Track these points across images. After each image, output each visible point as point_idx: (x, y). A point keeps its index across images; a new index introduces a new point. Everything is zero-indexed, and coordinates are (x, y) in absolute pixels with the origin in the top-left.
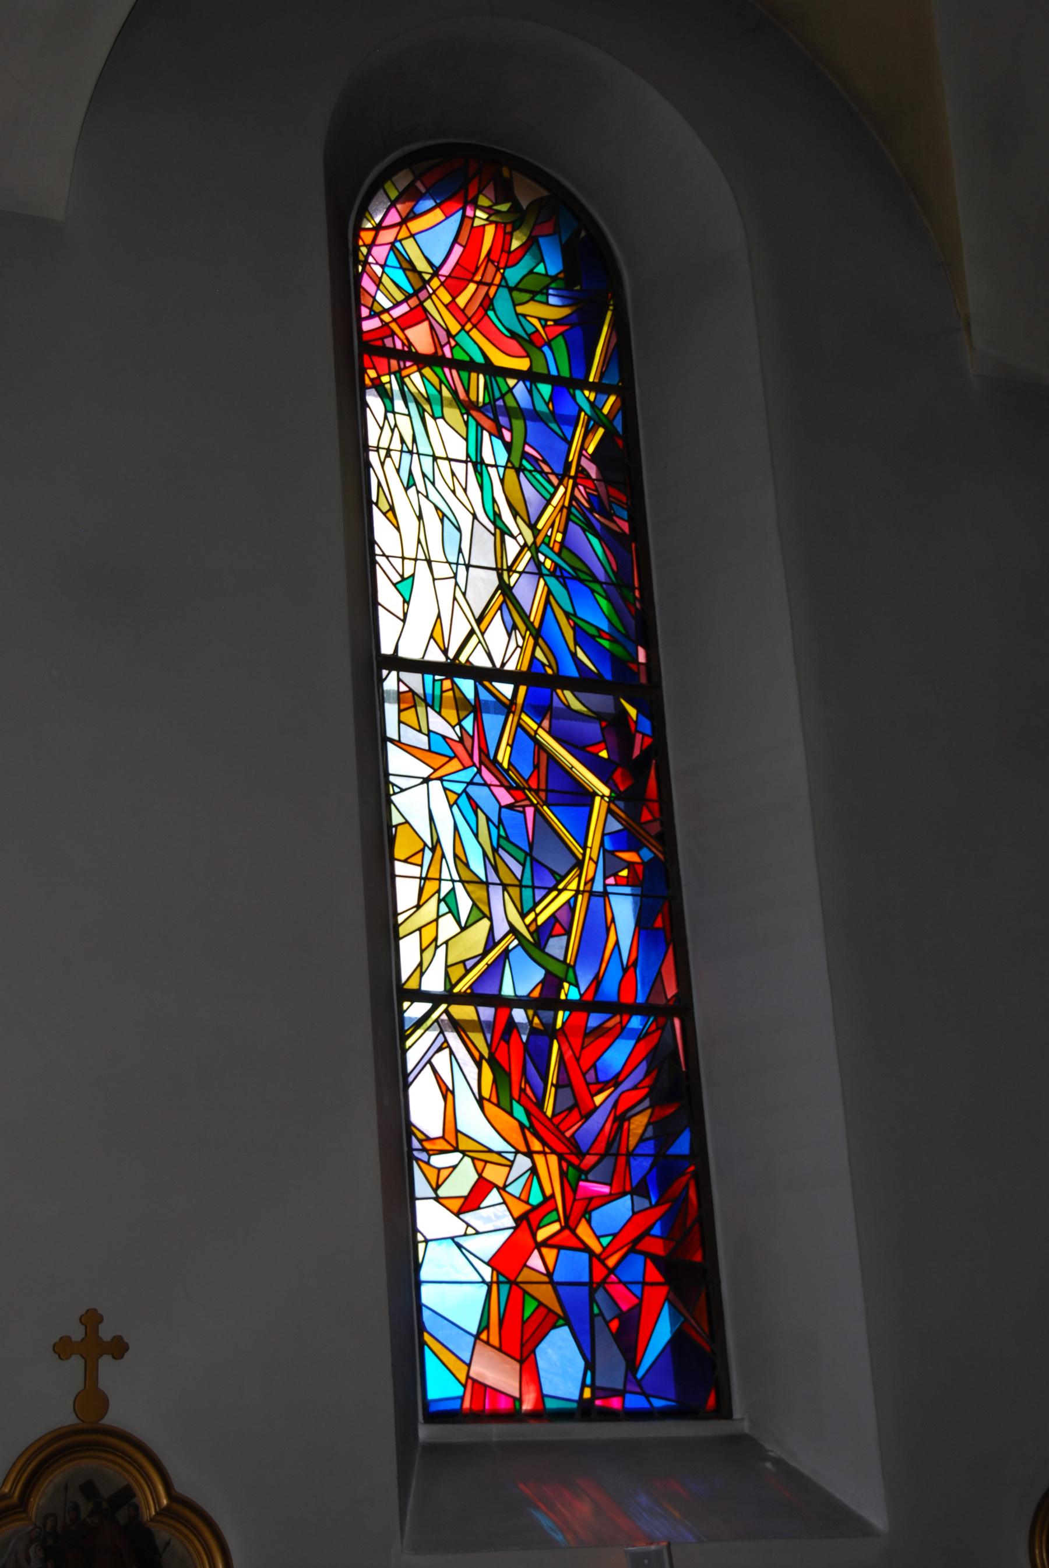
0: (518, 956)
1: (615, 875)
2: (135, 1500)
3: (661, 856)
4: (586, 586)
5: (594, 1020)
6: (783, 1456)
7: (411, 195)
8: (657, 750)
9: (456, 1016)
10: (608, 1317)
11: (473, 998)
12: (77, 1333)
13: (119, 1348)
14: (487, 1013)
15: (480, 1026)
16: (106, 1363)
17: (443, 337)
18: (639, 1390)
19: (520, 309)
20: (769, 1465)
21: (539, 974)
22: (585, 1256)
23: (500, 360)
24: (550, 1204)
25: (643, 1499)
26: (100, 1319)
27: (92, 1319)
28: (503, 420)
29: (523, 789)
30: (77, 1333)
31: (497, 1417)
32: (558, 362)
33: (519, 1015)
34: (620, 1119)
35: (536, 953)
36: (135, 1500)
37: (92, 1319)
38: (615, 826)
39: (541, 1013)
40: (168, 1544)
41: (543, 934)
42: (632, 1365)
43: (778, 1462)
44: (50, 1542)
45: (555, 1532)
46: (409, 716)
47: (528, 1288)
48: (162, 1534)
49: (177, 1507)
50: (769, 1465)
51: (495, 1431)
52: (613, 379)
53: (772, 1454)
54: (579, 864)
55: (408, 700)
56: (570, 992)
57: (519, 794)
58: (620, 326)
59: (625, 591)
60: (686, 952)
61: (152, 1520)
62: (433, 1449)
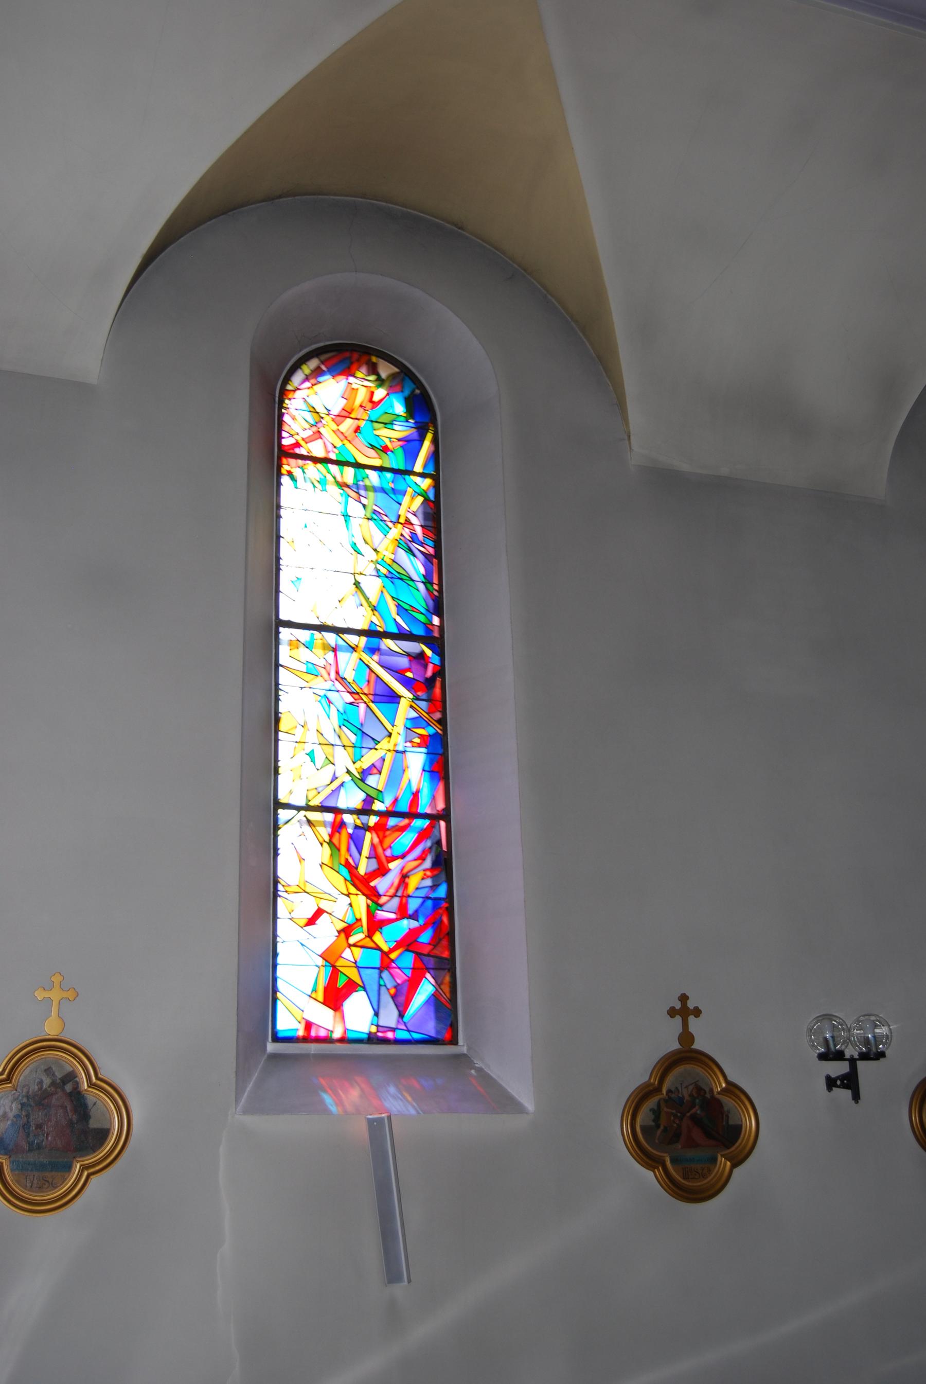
0: (350, 785)
1: (411, 742)
2: (77, 1079)
3: (439, 731)
4: (405, 582)
5: (392, 822)
6: (483, 1067)
7: (317, 373)
8: (440, 672)
9: (309, 818)
10: (389, 986)
11: (323, 809)
12: (678, 1006)
13: (697, 1012)
14: (329, 817)
15: (324, 824)
16: (691, 1019)
17: (330, 447)
18: (405, 1028)
19: (377, 433)
20: (473, 1072)
21: (363, 796)
22: (378, 953)
23: (362, 460)
24: (359, 923)
25: (392, 1089)
26: (687, 998)
27: (684, 998)
28: (362, 492)
29: (358, 693)
30: (678, 1006)
31: (319, 1040)
32: (397, 460)
33: (348, 819)
34: (404, 877)
35: (361, 784)
36: (77, 1079)
37: (684, 998)
38: (414, 714)
39: (361, 817)
40: (95, 1104)
41: (365, 773)
42: (401, 1015)
43: (479, 1070)
44: (25, 1100)
45: (332, 1105)
46: (295, 653)
47: (340, 968)
48: (724, 1099)
49: (732, 1088)
50: (473, 1072)
51: (313, 1048)
52: (431, 470)
53: (477, 1065)
54: (390, 735)
55: (295, 644)
56: (377, 806)
57: (356, 696)
58: (435, 441)
59: (429, 585)
60: (449, 784)
61: (719, 1093)
62: (274, 1057)
